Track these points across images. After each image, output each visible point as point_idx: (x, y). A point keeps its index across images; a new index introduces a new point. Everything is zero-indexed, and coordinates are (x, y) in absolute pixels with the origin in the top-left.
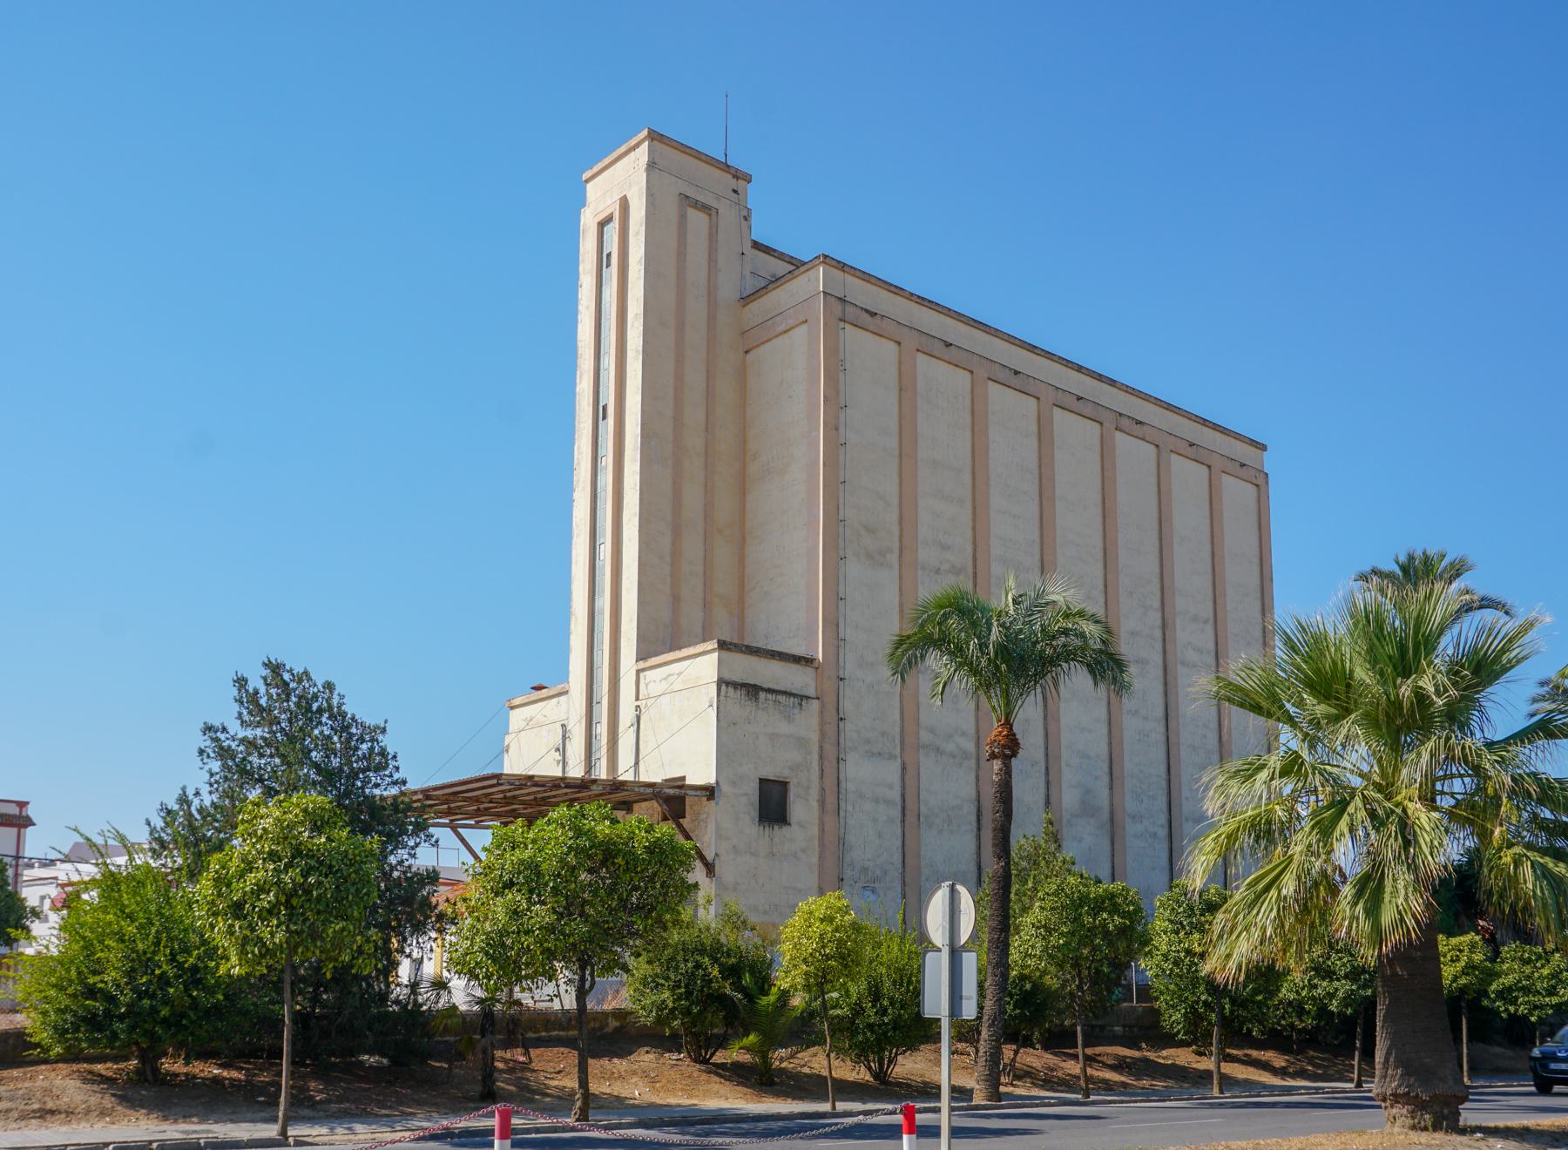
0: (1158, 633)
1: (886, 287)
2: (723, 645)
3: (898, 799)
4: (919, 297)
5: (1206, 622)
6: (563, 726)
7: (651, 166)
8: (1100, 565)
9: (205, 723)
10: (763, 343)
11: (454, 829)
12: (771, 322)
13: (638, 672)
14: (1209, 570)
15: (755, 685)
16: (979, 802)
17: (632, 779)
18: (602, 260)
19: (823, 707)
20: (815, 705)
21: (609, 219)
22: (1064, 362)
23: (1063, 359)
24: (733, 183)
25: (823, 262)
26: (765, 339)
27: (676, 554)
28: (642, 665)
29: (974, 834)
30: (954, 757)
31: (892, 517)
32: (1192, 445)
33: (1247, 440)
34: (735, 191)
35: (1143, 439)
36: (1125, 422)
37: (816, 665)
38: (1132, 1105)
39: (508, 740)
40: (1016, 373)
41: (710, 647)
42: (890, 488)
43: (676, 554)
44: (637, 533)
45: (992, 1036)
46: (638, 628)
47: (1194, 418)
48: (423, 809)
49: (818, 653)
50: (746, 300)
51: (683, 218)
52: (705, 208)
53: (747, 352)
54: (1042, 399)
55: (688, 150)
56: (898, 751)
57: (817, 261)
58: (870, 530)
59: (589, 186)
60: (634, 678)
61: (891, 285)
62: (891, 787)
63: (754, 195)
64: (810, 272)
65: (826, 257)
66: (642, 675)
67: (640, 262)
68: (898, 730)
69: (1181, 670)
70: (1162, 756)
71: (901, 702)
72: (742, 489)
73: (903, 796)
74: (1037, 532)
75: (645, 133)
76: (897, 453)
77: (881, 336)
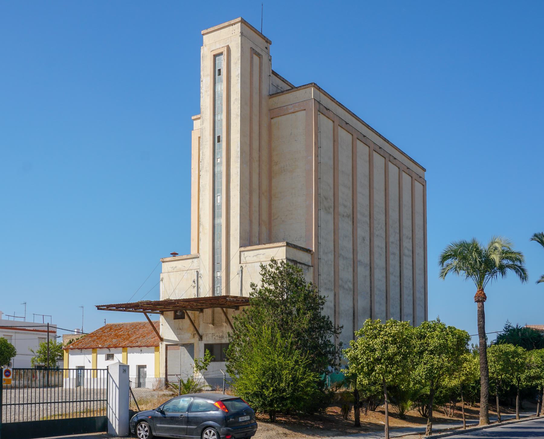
0: (398, 242)
1: (330, 98)
2: (288, 245)
3: (333, 307)
4: (339, 103)
5: (410, 239)
6: (197, 272)
7: (242, 34)
8: (384, 215)
9: (251, 283)
10: (281, 116)
11: (145, 314)
12: (285, 107)
13: (240, 252)
14: (411, 218)
15: (296, 261)
16: (354, 308)
17: (240, 296)
18: (217, 72)
19: (314, 270)
20: (312, 269)
21: (221, 54)
22: (376, 133)
23: (376, 131)
24: (266, 44)
25: (314, 86)
26: (282, 114)
27: (250, 203)
28: (243, 249)
29: (352, 321)
30: (347, 290)
31: (331, 194)
32: (408, 168)
33: (421, 167)
34: (266, 48)
35: (395, 165)
36: (392, 158)
37: (312, 253)
38: (519, 423)
39: (162, 276)
40: (364, 136)
41: (283, 245)
42: (331, 181)
43: (250, 203)
44: (239, 193)
45: (486, 400)
46: (240, 233)
47: (408, 157)
48: (185, 308)
49: (312, 248)
50: (271, 96)
51: (252, 58)
52: (259, 55)
53: (272, 118)
54: (371, 147)
55: (253, 29)
56: (333, 288)
57: (311, 85)
58: (326, 199)
59: (204, 37)
60: (239, 254)
61: (332, 97)
62: (331, 302)
63: (272, 49)
64: (307, 89)
65: (314, 84)
66: (242, 253)
67: (238, 76)
68: (333, 279)
69: (404, 257)
70: (398, 291)
71: (334, 268)
72: (270, 178)
73: (335, 306)
74: (368, 201)
75: (239, 19)
76: (333, 167)
77: (329, 118)
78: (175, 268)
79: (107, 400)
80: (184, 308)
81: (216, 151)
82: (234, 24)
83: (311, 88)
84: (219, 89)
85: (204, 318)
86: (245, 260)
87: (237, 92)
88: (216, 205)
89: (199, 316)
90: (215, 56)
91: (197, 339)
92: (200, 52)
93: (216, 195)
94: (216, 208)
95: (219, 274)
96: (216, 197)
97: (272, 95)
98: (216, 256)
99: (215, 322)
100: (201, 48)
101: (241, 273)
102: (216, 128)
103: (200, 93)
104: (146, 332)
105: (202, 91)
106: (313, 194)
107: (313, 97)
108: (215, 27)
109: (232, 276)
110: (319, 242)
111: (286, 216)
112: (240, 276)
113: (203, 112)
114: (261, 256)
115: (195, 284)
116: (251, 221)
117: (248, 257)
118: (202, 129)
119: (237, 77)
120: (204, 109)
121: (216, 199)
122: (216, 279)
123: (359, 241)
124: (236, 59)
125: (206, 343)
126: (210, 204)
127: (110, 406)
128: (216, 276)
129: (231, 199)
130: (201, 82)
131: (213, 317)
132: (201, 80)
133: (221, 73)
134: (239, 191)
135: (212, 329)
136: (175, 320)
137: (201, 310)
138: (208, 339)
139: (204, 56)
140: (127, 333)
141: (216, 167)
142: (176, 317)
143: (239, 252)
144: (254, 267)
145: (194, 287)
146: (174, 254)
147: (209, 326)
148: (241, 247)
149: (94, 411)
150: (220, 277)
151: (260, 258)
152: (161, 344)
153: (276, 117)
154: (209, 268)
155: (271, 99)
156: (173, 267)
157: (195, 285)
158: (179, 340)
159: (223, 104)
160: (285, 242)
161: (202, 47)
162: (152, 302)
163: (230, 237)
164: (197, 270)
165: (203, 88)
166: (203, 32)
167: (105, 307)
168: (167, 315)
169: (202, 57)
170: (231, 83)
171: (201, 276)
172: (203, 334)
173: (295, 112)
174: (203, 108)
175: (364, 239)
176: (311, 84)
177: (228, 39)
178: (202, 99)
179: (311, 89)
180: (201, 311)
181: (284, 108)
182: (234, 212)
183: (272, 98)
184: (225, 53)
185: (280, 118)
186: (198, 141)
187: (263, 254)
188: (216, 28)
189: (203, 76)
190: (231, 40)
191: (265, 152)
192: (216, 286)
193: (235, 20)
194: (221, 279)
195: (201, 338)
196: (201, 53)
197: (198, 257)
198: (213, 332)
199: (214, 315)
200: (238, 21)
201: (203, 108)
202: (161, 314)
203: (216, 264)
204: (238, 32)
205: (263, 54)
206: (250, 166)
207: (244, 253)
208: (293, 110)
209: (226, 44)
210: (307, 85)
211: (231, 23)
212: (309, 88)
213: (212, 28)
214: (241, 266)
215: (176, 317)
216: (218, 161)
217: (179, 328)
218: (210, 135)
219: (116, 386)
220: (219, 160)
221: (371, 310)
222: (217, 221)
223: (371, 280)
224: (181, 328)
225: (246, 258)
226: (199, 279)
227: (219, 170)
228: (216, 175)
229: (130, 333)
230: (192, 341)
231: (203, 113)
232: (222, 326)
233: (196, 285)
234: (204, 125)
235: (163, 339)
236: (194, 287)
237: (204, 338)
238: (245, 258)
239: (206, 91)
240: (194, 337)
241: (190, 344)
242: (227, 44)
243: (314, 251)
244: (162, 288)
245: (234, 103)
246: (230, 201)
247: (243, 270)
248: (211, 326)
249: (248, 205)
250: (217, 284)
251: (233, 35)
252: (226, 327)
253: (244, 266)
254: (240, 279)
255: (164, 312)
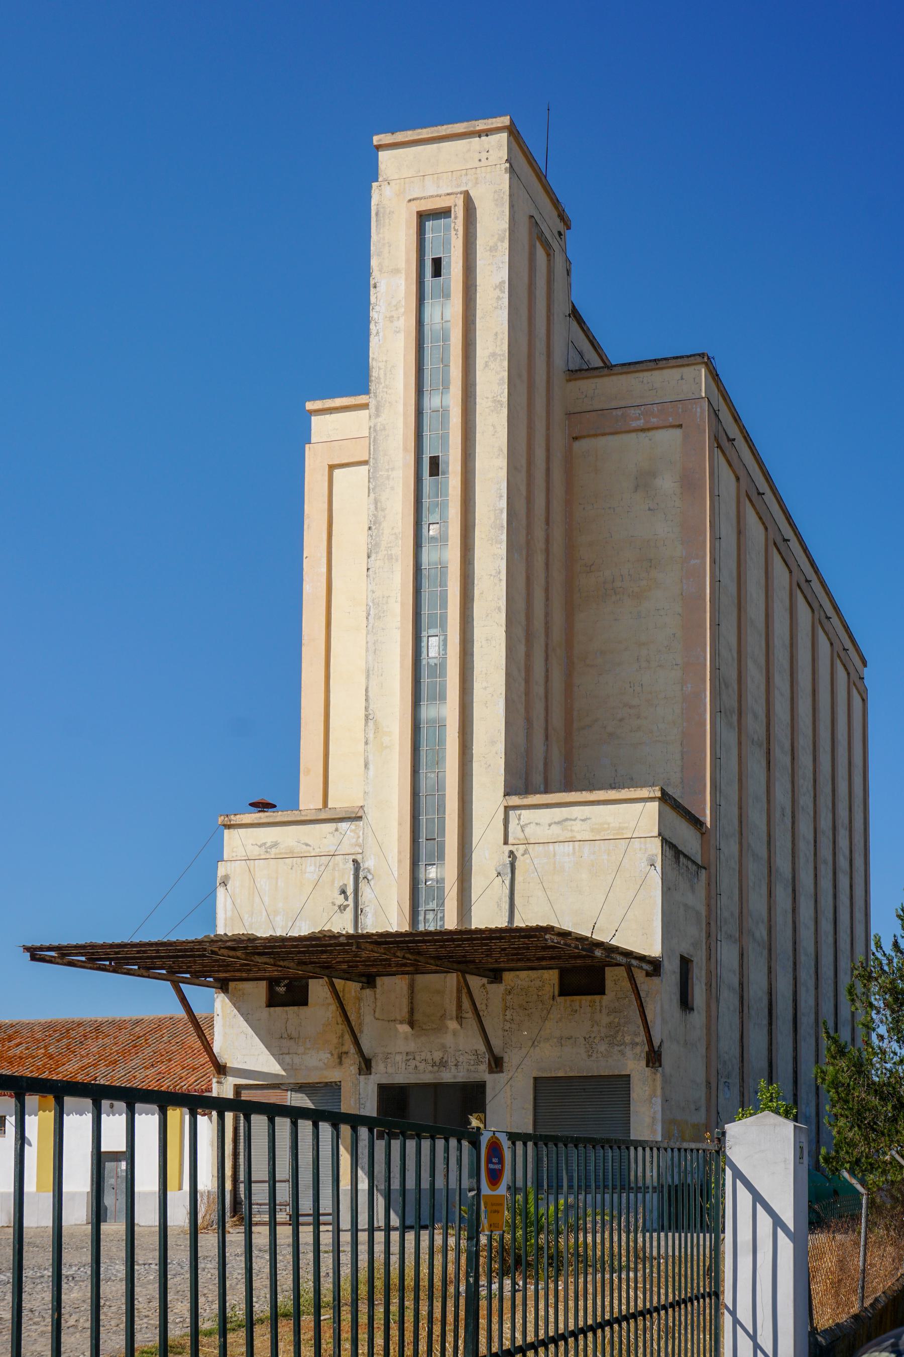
10: (604, 434)
11: (173, 982)
12: (619, 412)
13: (507, 809)
24: (561, 227)
27: (528, 669)
28: (515, 800)
34: (560, 234)
39: (222, 869)
41: (652, 795)
43: (528, 669)
50: (574, 374)
53: (576, 439)
57: (699, 359)
64: (685, 370)
75: (505, 121)
78: (271, 847)
79: (717, 1295)
80: (327, 971)
81: (426, 501)
82: (487, 133)
83: (697, 367)
84: (437, 319)
85: (379, 1004)
86: (521, 836)
87: (496, 334)
88: (424, 662)
89: (359, 999)
90: (423, 217)
91: (354, 1069)
92: (370, 197)
93: (424, 634)
94: (425, 673)
95: (432, 872)
96: (425, 639)
97: (576, 371)
98: (423, 818)
99: (417, 1016)
100: (371, 187)
101: (509, 870)
102: (426, 433)
103: (369, 322)
104: (115, 1048)
105: (373, 314)
106: (705, 665)
107: (703, 395)
108: (420, 131)
109: (477, 883)
110: (718, 803)
111: (621, 720)
112: (507, 882)
113: (378, 378)
114: (577, 826)
115: (346, 898)
116: (529, 720)
117: (532, 826)
118: (375, 430)
119: (498, 290)
120: (382, 372)
121: (424, 644)
122: (422, 886)
123: (778, 814)
124: (493, 236)
125: (384, 1081)
126: (403, 657)
127: (736, 1322)
128: (422, 876)
129: (475, 650)
130: (372, 291)
131: (412, 1003)
132: (372, 282)
133: (443, 271)
134: (504, 628)
135: (406, 1038)
136: (272, 1009)
137: (369, 981)
138: (390, 1070)
139: (381, 210)
140: (42, 1051)
141: (424, 550)
142: (273, 1001)
143: (502, 809)
144: (555, 855)
145: (342, 908)
146: (263, 806)
147: (396, 1029)
148: (506, 794)
149: (250, 1323)
150: (440, 881)
151: (571, 831)
152: (218, 1082)
153: (589, 436)
154: (399, 852)
155: (573, 383)
156: (265, 844)
157: (346, 903)
158: (284, 1070)
159: (452, 364)
160: (657, 788)
161: (374, 184)
162: (257, 938)
163: (471, 761)
164: (354, 857)
165: (377, 308)
166: (380, 140)
167: (53, 954)
168: (243, 994)
169: (377, 214)
170: (478, 306)
171: (370, 877)
172: (375, 1055)
173: (649, 429)
174: (380, 369)
175: (783, 809)
176: (702, 355)
177: (466, 174)
178: (374, 342)
179: (700, 371)
180: (368, 983)
181: (614, 412)
182: (485, 688)
183: (576, 379)
184: (459, 212)
185: (602, 441)
186: (326, 478)
187: (583, 820)
188: (425, 133)
189: (380, 271)
190: (477, 179)
191: (558, 533)
192: (422, 909)
193: (490, 121)
194: (441, 889)
195: (366, 1065)
196: (374, 202)
197: (360, 818)
198: (412, 1046)
199: (412, 999)
200: (500, 125)
201: (380, 369)
202: (221, 988)
203: (422, 840)
204: (500, 158)
205: (555, 245)
206: (527, 559)
207: (518, 812)
208: (642, 421)
209: (458, 186)
210: (688, 357)
211: (478, 128)
212: (692, 368)
213: (410, 133)
214: (511, 852)
215: (273, 1001)
216: (431, 533)
217: (285, 1035)
218: (405, 449)
219: (778, 1222)
220: (434, 531)
221: (796, 1005)
222: (427, 712)
223: (794, 923)
224: (294, 1034)
225: (528, 830)
226: (362, 884)
227: (435, 557)
228: (425, 572)
229: (52, 1050)
230: (333, 1075)
231: (379, 383)
232: (441, 1029)
233: (351, 901)
234: (380, 419)
235: (225, 1067)
236: (342, 908)
237: (379, 1067)
238: (522, 827)
239: (391, 319)
240: (340, 1063)
241: (327, 1083)
242: (464, 189)
243: (709, 826)
244: (225, 906)
245: (486, 365)
246: (472, 655)
247: (517, 864)
248: (404, 1028)
249: (523, 674)
250: (427, 903)
251: (481, 164)
252: (455, 1033)
253: (519, 851)
254: (507, 892)
255: (232, 985)
